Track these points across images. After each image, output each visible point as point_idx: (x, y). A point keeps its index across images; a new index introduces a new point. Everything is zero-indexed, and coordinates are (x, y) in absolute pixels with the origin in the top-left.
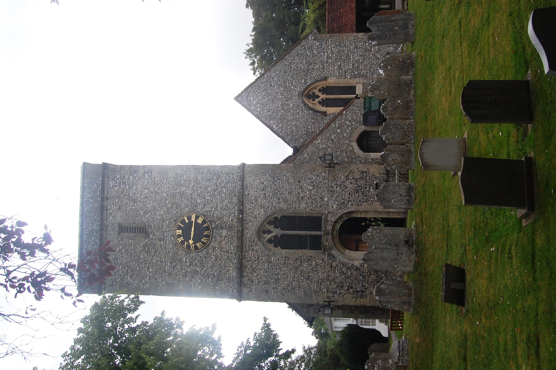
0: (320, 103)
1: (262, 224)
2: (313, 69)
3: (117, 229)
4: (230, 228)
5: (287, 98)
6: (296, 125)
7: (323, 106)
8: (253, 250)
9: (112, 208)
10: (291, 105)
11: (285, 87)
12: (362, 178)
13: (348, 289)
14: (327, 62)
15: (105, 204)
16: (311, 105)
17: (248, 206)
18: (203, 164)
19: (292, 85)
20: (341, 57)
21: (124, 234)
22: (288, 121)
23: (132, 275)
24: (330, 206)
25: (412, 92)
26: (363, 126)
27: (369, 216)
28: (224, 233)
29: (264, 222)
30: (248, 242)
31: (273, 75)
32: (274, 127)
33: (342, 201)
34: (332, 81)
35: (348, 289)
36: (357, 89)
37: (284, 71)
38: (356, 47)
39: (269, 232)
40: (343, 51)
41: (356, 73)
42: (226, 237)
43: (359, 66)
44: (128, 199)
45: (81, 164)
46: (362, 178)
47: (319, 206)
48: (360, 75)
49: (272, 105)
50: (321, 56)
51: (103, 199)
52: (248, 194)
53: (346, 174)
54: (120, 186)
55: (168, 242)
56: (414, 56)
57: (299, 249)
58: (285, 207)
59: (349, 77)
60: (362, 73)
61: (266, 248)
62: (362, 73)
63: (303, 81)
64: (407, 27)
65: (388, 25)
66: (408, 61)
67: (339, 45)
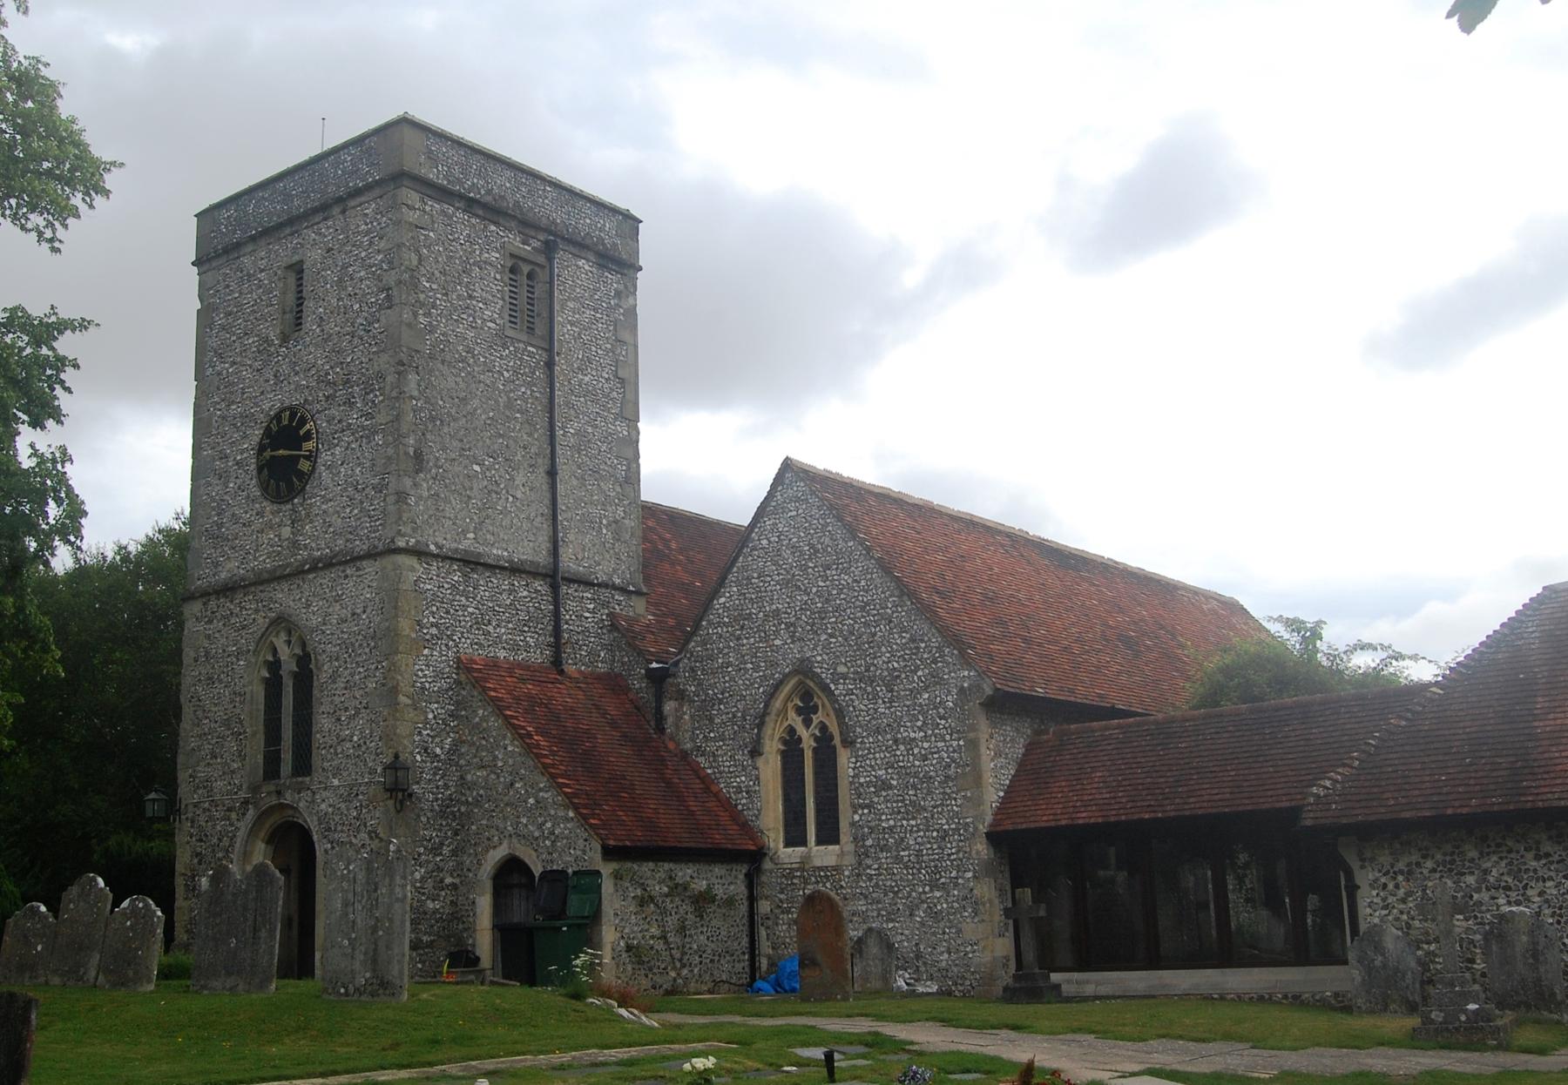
2: (876, 696)
5: (792, 624)
6: (729, 664)
8: (257, 611)
9: (328, 230)
10: (777, 642)
11: (823, 614)
13: (198, 854)
14: (896, 741)
15: (336, 210)
16: (778, 704)
17: (325, 579)
18: (190, 461)
19: (831, 636)
20: (914, 787)
22: (738, 639)
25: (56, 980)
26: (541, 870)
28: (286, 532)
32: (722, 600)
34: (844, 759)
36: (831, 847)
37: (867, 604)
38: (944, 836)
40: (930, 792)
41: (869, 842)
48: (862, 854)
49: (778, 583)
50: (915, 719)
51: (340, 200)
52: (346, 577)
56: (141, 989)
57: (266, 726)
59: (857, 817)
60: (869, 862)
62: (869, 862)
63: (842, 669)
64: (229, 974)
65: (246, 920)
66: (131, 973)
67: (947, 777)
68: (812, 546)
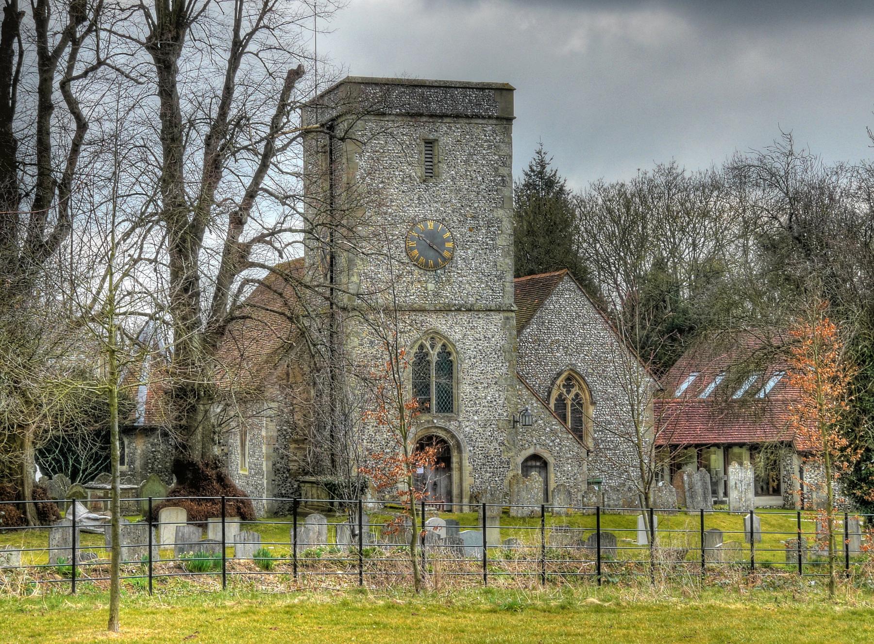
0: (560, 395)
1: (444, 337)
3: (431, 137)
4: (437, 295)
7: (556, 400)
12: (501, 463)
16: (558, 382)
21: (423, 147)
23: (373, 159)
24: (467, 424)
27: (455, 475)
28: (431, 286)
29: (447, 338)
30: (421, 319)
31: (599, 327)
33: (474, 438)
34: (592, 411)
35: (368, 450)
39: (432, 347)
42: (426, 289)
43: (610, 449)
44: (470, 154)
45: (513, 84)
46: (501, 463)
47: (468, 409)
53: (506, 442)
54: (486, 141)
55: (417, 209)
58: (465, 366)
61: (415, 342)
63: (590, 370)
68: (577, 313)
